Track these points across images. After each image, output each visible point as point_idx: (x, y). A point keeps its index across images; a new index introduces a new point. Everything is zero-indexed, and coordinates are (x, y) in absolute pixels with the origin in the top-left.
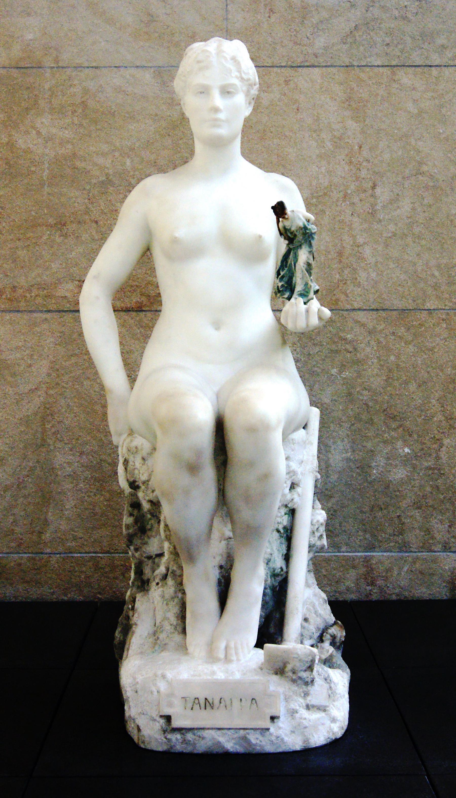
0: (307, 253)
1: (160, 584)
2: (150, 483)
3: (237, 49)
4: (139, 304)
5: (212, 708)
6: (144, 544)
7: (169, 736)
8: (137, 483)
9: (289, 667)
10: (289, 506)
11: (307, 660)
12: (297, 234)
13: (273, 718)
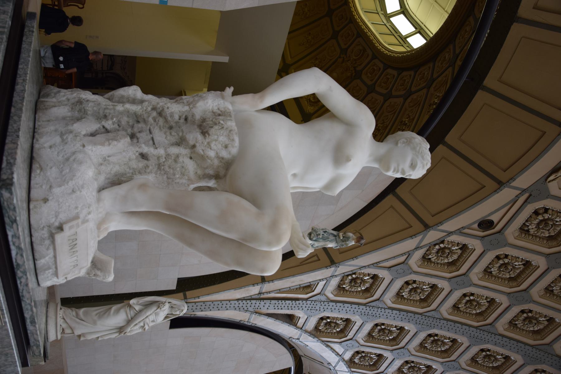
2: (209, 150)
3: (417, 174)
4: (306, 110)
7: (46, 229)
9: (99, 273)
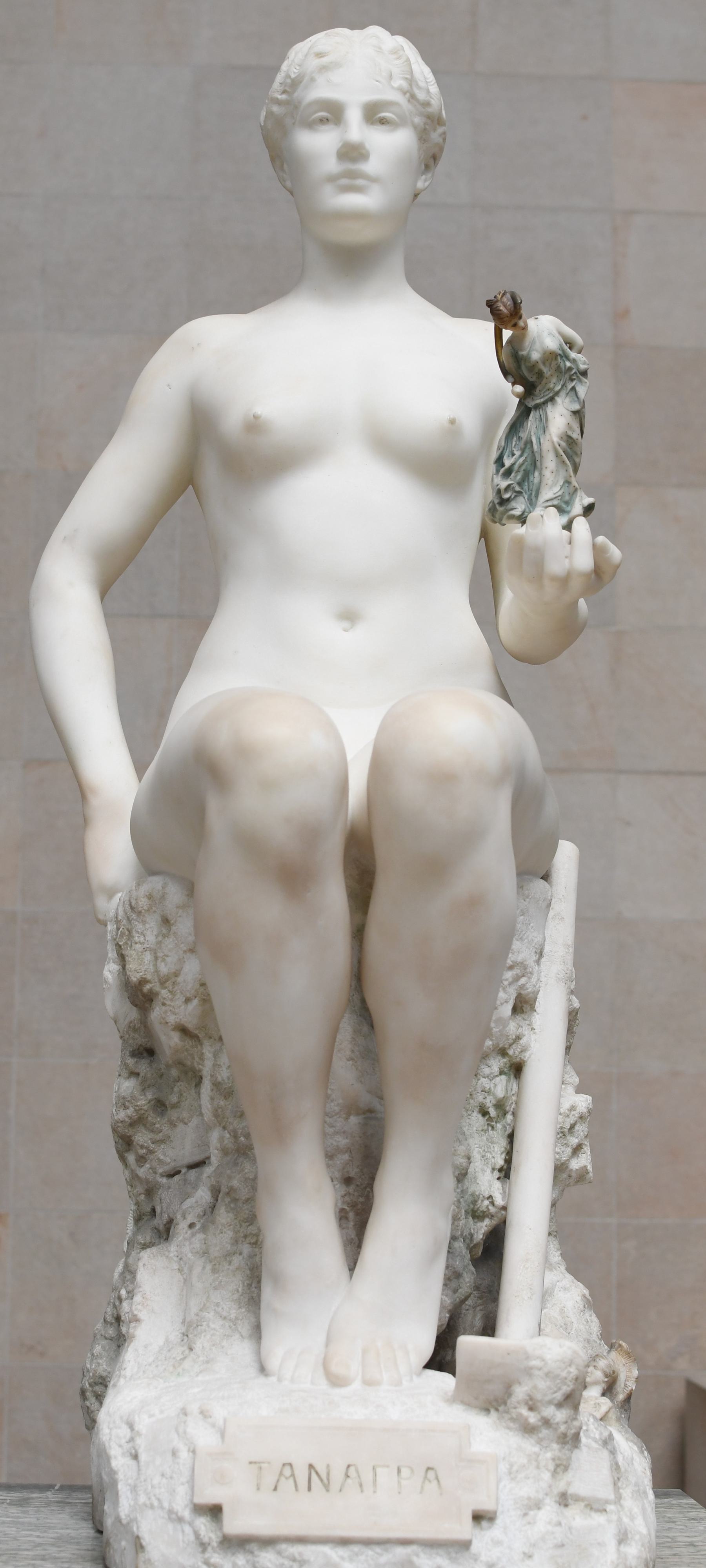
0: (568, 414)
1: (198, 1226)
2: (180, 979)
5: (327, 1487)
6: (162, 1141)
8: (147, 988)
9: (520, 1392)
10: (511, 1052)
11: (564, 1374)
12: (545, 370)
13: (478, 1518)
